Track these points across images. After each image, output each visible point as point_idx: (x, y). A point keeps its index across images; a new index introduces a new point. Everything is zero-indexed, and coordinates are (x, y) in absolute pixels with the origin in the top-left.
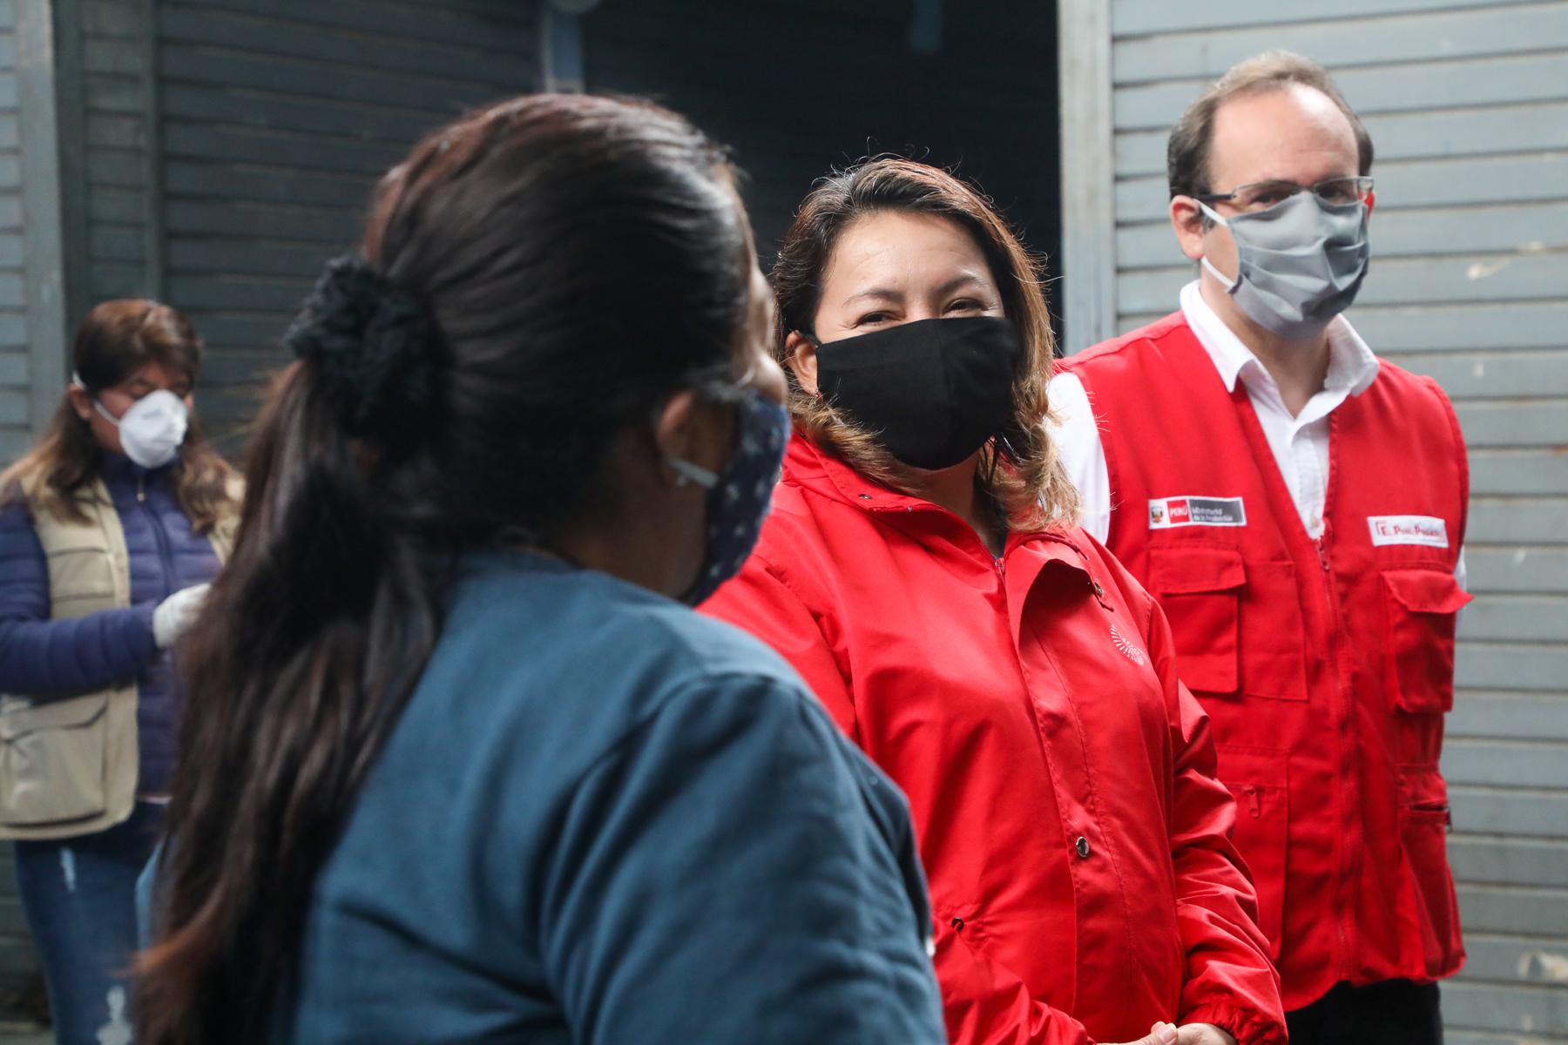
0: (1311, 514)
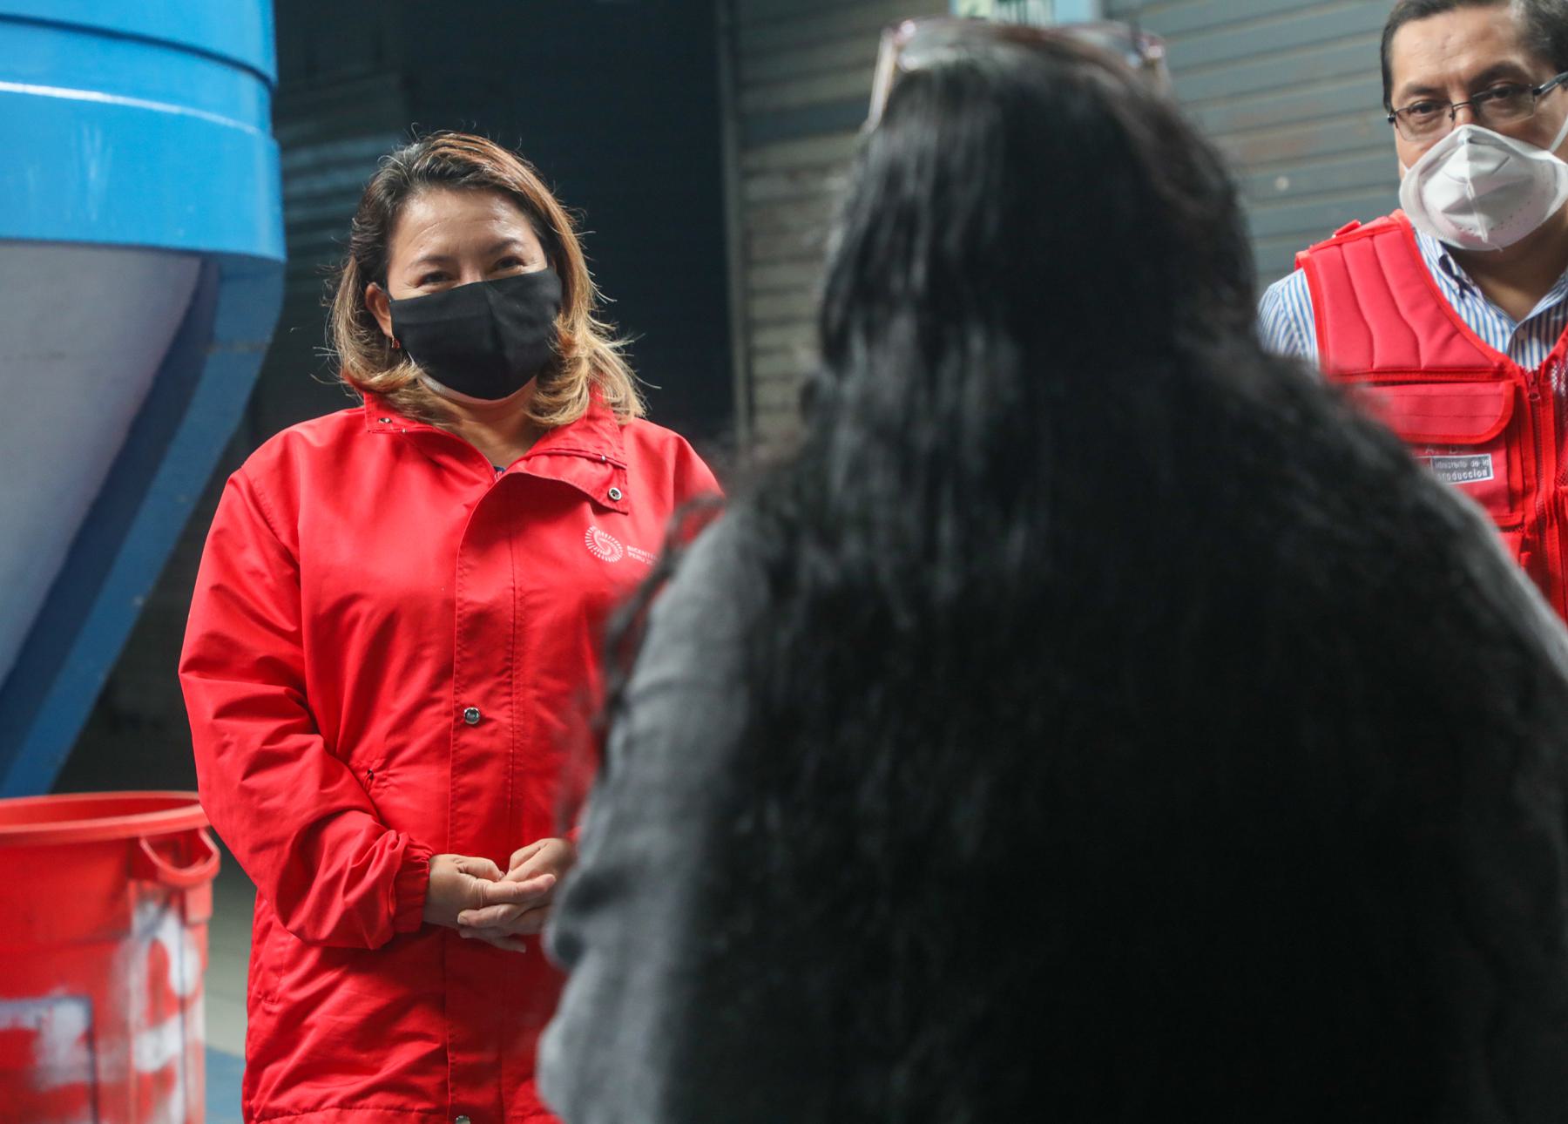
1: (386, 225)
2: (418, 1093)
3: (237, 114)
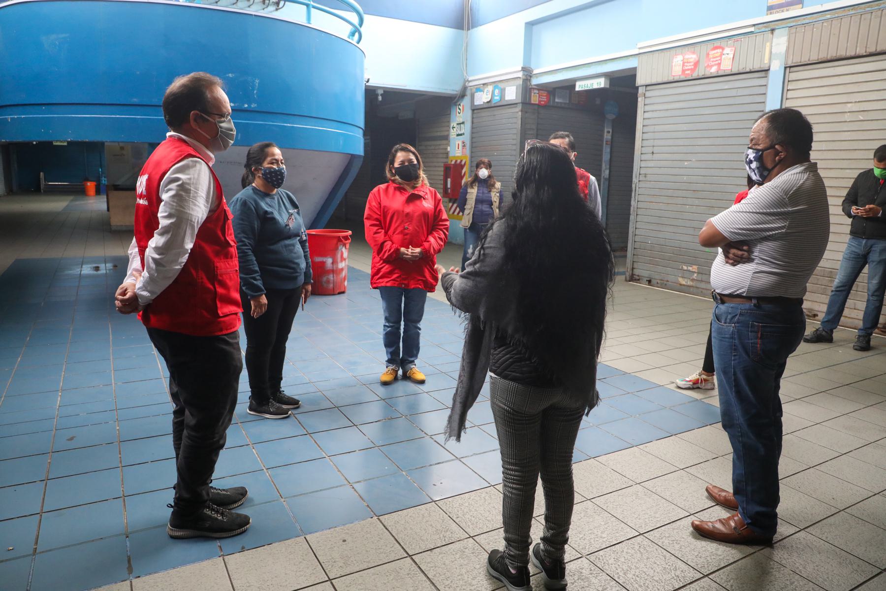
1: (394, 156)
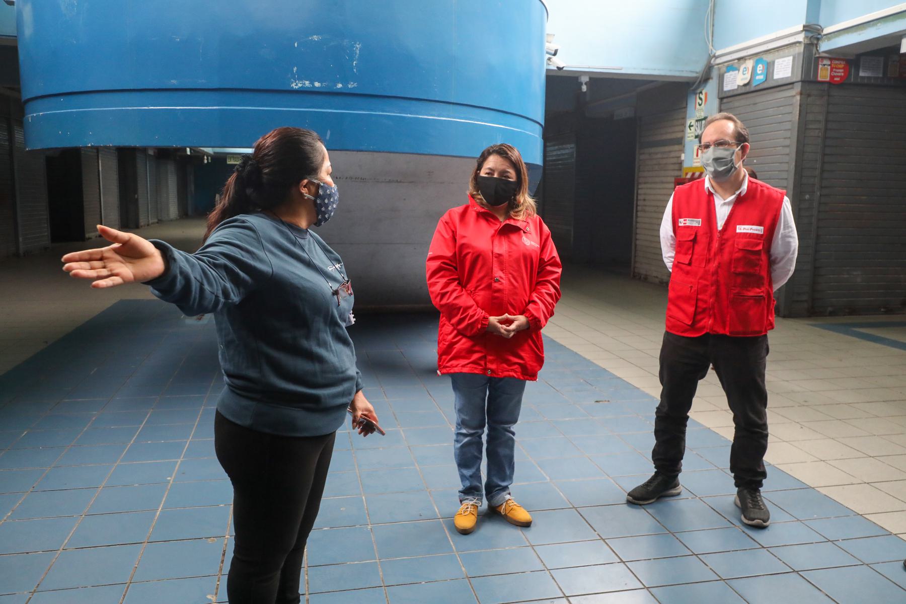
0: (720, 224)
2: (480, 365)
3: (535, 134)
